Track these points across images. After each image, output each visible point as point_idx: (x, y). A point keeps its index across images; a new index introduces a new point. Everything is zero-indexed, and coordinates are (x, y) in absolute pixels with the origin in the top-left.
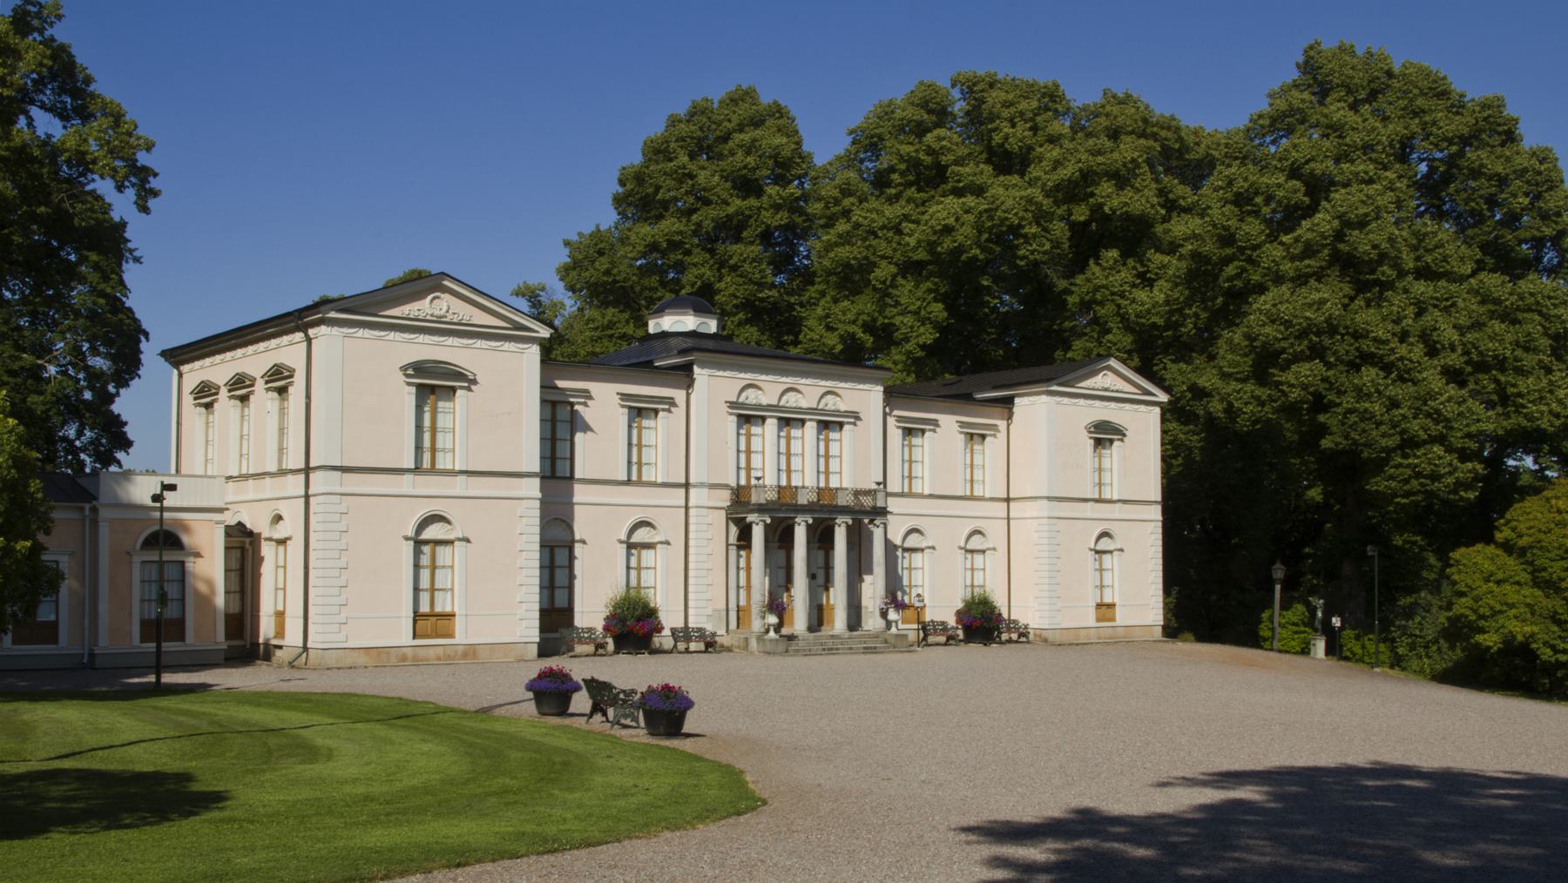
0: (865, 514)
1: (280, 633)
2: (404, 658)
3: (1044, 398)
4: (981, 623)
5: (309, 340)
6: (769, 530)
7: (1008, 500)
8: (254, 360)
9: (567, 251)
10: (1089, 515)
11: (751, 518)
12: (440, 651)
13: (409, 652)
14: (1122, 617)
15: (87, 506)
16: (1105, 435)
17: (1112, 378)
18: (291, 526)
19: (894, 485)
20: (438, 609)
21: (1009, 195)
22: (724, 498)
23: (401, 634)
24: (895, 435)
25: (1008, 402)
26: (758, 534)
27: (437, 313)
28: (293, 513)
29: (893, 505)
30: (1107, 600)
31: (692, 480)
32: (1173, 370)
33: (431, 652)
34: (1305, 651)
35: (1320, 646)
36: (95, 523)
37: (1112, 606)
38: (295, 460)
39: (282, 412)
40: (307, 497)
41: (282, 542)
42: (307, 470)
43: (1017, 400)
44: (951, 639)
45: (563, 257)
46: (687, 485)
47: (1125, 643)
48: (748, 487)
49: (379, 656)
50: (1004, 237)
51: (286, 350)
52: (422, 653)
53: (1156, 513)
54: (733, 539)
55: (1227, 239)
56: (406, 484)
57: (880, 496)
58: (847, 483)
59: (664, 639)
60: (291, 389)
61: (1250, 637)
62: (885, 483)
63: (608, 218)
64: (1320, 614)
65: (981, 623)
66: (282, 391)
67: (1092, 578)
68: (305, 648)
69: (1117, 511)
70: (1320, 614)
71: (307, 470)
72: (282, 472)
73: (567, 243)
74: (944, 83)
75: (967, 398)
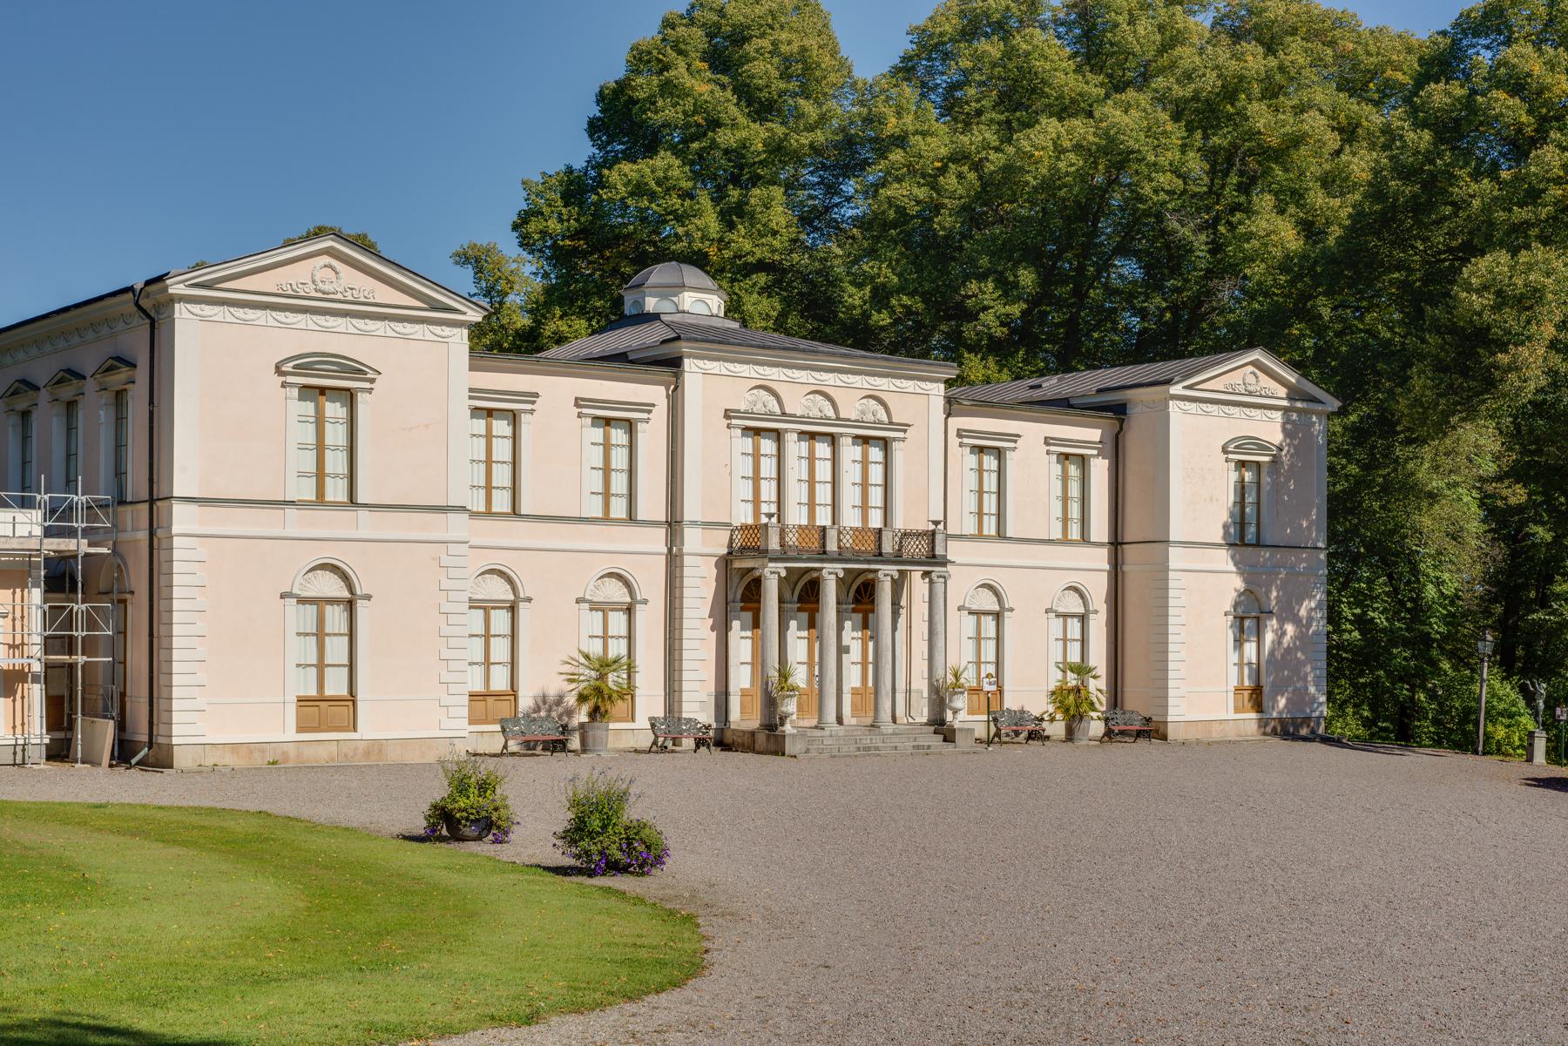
12: (333, 748)
13: (291, 749)
22: (719, 544)
25: (1115, 411)
29: (954, 551)
49: (274, 765)
57: (939, 538)
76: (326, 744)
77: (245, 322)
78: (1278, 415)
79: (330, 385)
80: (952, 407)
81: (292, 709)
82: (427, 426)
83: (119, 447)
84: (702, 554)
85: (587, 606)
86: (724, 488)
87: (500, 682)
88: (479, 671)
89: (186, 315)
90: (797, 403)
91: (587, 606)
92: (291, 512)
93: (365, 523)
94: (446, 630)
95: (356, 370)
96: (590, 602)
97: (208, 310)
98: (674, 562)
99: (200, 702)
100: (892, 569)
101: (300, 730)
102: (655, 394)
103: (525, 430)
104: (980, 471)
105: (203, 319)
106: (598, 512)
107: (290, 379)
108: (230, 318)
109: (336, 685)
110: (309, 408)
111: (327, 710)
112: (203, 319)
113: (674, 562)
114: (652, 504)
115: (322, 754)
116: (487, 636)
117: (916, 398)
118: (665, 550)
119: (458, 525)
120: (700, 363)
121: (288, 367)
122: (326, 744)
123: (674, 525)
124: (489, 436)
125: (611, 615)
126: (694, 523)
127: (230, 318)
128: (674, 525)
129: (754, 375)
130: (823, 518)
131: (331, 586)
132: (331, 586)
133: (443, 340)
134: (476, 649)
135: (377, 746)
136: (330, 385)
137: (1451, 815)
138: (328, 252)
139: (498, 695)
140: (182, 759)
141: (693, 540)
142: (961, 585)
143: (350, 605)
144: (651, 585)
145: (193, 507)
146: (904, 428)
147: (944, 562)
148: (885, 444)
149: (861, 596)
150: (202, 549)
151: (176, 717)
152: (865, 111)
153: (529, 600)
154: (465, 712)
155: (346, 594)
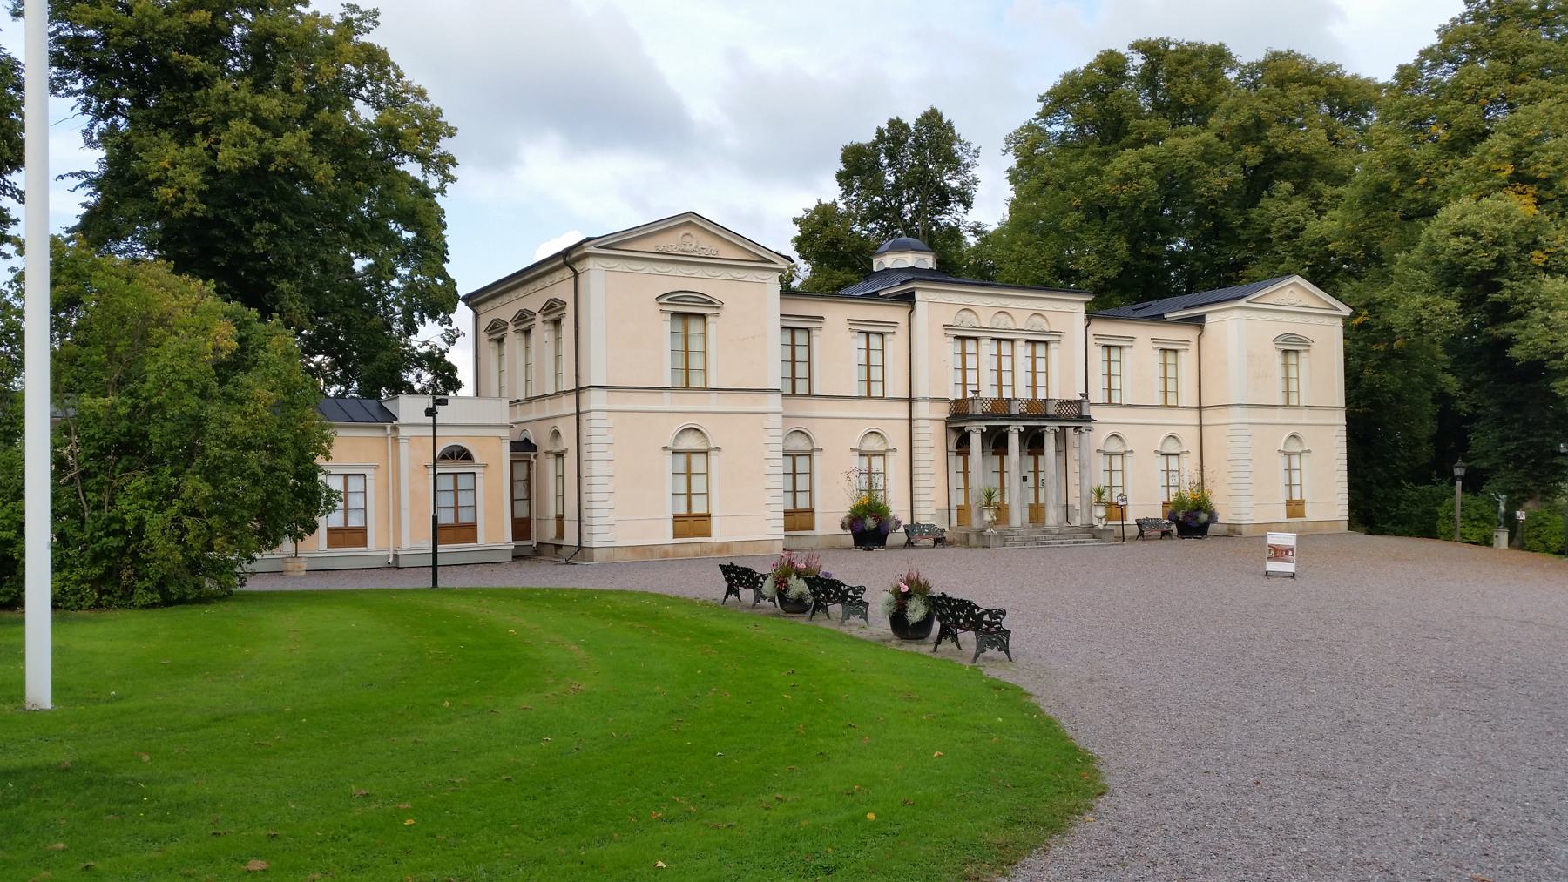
0: (1076, 415)
1: (560, 534)
2: (666, 554)
3: (1236, 314)
4: (1190, 520)
5: (576, 275)
6: (985, 436)
7: (1200, 408)
8: (533, 300)
9: (797, 228)
10: (1277, 420)
11: (968, 427)
12: (697, 548)
13: (670, 548)
14: (1311, 513)
15: (389, 426)
16: (1291, 348)
17: (1295, 292)
18: (567, 441)
19: (1097, 395)
20: (695, 511)
21: (1186, 143)
22: (943, 411)
23: (663, 535)
24: (1097, 355)
25: (1198, 321)
26: (976, 441)
27: (687, 248)
28: (567, 429)
29: (1094, 413)
30: (1296, 497)
31: (918, 393)
32: (1347, 288)
33: (690, 550)
34: (1487, 542)
35: (1502, 537)
36: (396, 439)
37: (1301, 502)
38: (568, 383)
39: (558, 340)
40: (578, 413)
41: (559, 455)
42: (578, 391)
43: (1208, 318)
44: (1166, 534)
45: (796, 231)
46: (911, 400)
47: (1311, 537)
48: (965, 400)
49: (645, 556)
50: (1175, 183)
51: (560, 287)
52: (681, 550)
53: (1340, 418)
54: (952, 446)
55: (1404, 167)
56: (667, 401)
57: (1085, 405)
58: (1055, 394)
59: (897, 536)
60: (563, 321)
61: (1427, 529)
62: (1086, 395)
63: (830, 192)
64: (1502, 508)
65: (1190, 520)
66: (557, 323)
67: (1282, 478)
68: (579, 546)
69: (1305, 417)
70: (1502, 508)
71: (578, 391)
72: (559, 394)
73: (796, 221)
74: (1123, 49)
75: (1159, 319)
78: (1340, 323)
80: (1090, 316)
81: (670, 523)
83: (557, 357)
84: (932, 418)
86: (940, 376)
92: (667, 394)
93: (713, 402)
97: (612, 263)
99: (611, 520)
100: (1055, 425)
101: (676, 536)
103: (815, 341)
104: (999, 356)
106: (864, 394)
110: (679, 327)
111: (691, 523)
117: (1066, 314)
121: (664, 300)
130: (1007, 394)
135: (726, 546)
137: (1475, 596)
141: (921, 409)
142: (1098, 436)
144: (896, 436)
145: (604, 392)
146: (1059, 334)
149: (1033, 443)
150: (611, 420)
152: (1204, 91)
154: (782, 523)
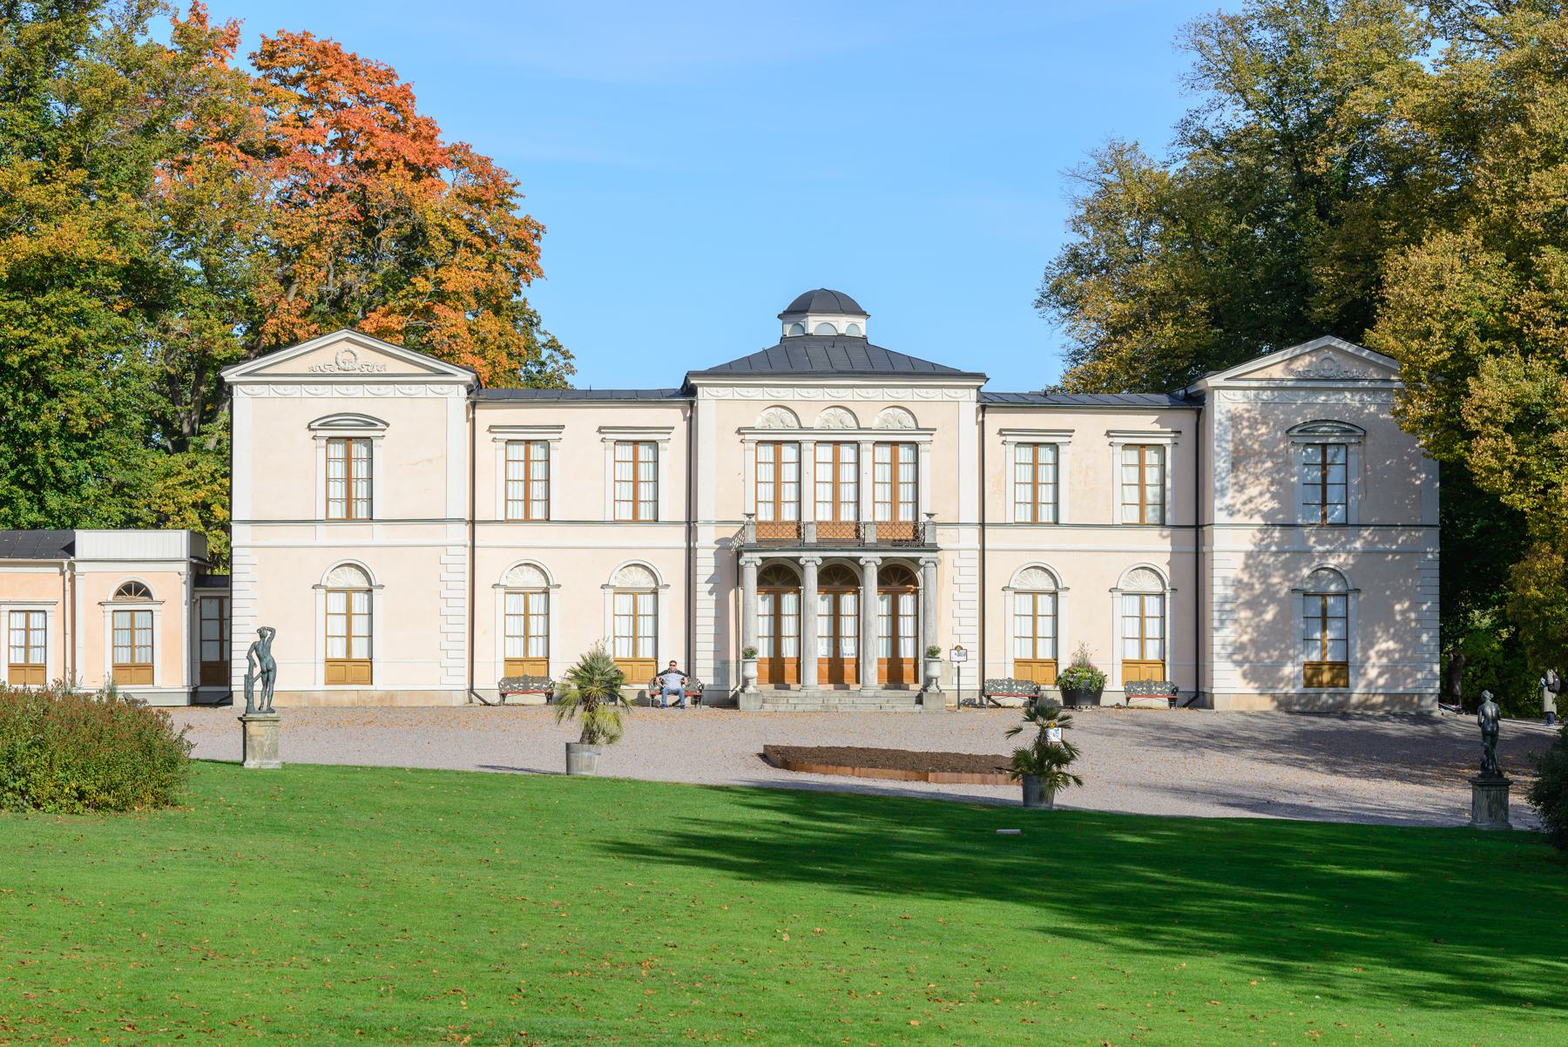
12: (354, 696)
76: (349, 693)
77: (285, 396)
79: (352, 437)
81: (321, 669)
82: (430, 461)
85: (611, 591)
86: (735, 490)
87: (1045, 652)
88: (520, 642)
89: (241, 394)
90: (814, 418)
91: (611, 591)
93: (379, 533)
94: (445, 611)
95: (370, 422)
96: (505, 587)
98: (690, 553)
102: (673, 416)
103: (923, 457)
105: (254, 397)
107: (320, 433)
108: (273, 394)
109: (359, 651)
112: (254, 397)
113: (690, 553)
114: (673, 507)
115: (346, 700)
116: (1035, 616)
118: (684, 545)
119: (323, 534)
120: (713, 390)
122: (349, 693)
123: (691, 524)
124: (1035, 464)
125: (641, 598)
126: (708, 523)
127: (273, 394)
128: (691, 524)
129: (827, 398)
131: (355, 579)
132: (355, 579)
133: (443, 397)
134: (1132, 628)
135: (391, 695)
136: (352, 437)
138: (348, 340)
139: (1043, 662)
140: (1217, 708)
143: (1055, 594)
144: (673, 574)
145: (248, 527)
146: (931, 431)
147: (934, 549)
148: (1055, 447)
151: (1216, 675)
153: (382, 587)
155: (1053, 588)
